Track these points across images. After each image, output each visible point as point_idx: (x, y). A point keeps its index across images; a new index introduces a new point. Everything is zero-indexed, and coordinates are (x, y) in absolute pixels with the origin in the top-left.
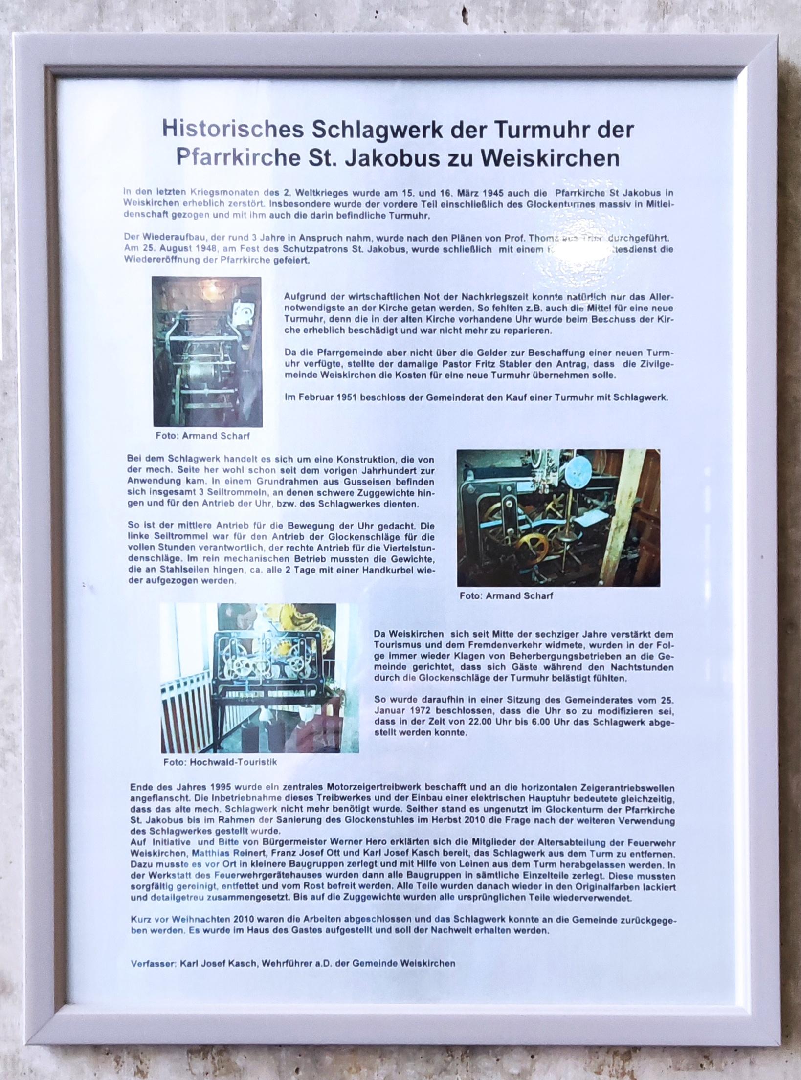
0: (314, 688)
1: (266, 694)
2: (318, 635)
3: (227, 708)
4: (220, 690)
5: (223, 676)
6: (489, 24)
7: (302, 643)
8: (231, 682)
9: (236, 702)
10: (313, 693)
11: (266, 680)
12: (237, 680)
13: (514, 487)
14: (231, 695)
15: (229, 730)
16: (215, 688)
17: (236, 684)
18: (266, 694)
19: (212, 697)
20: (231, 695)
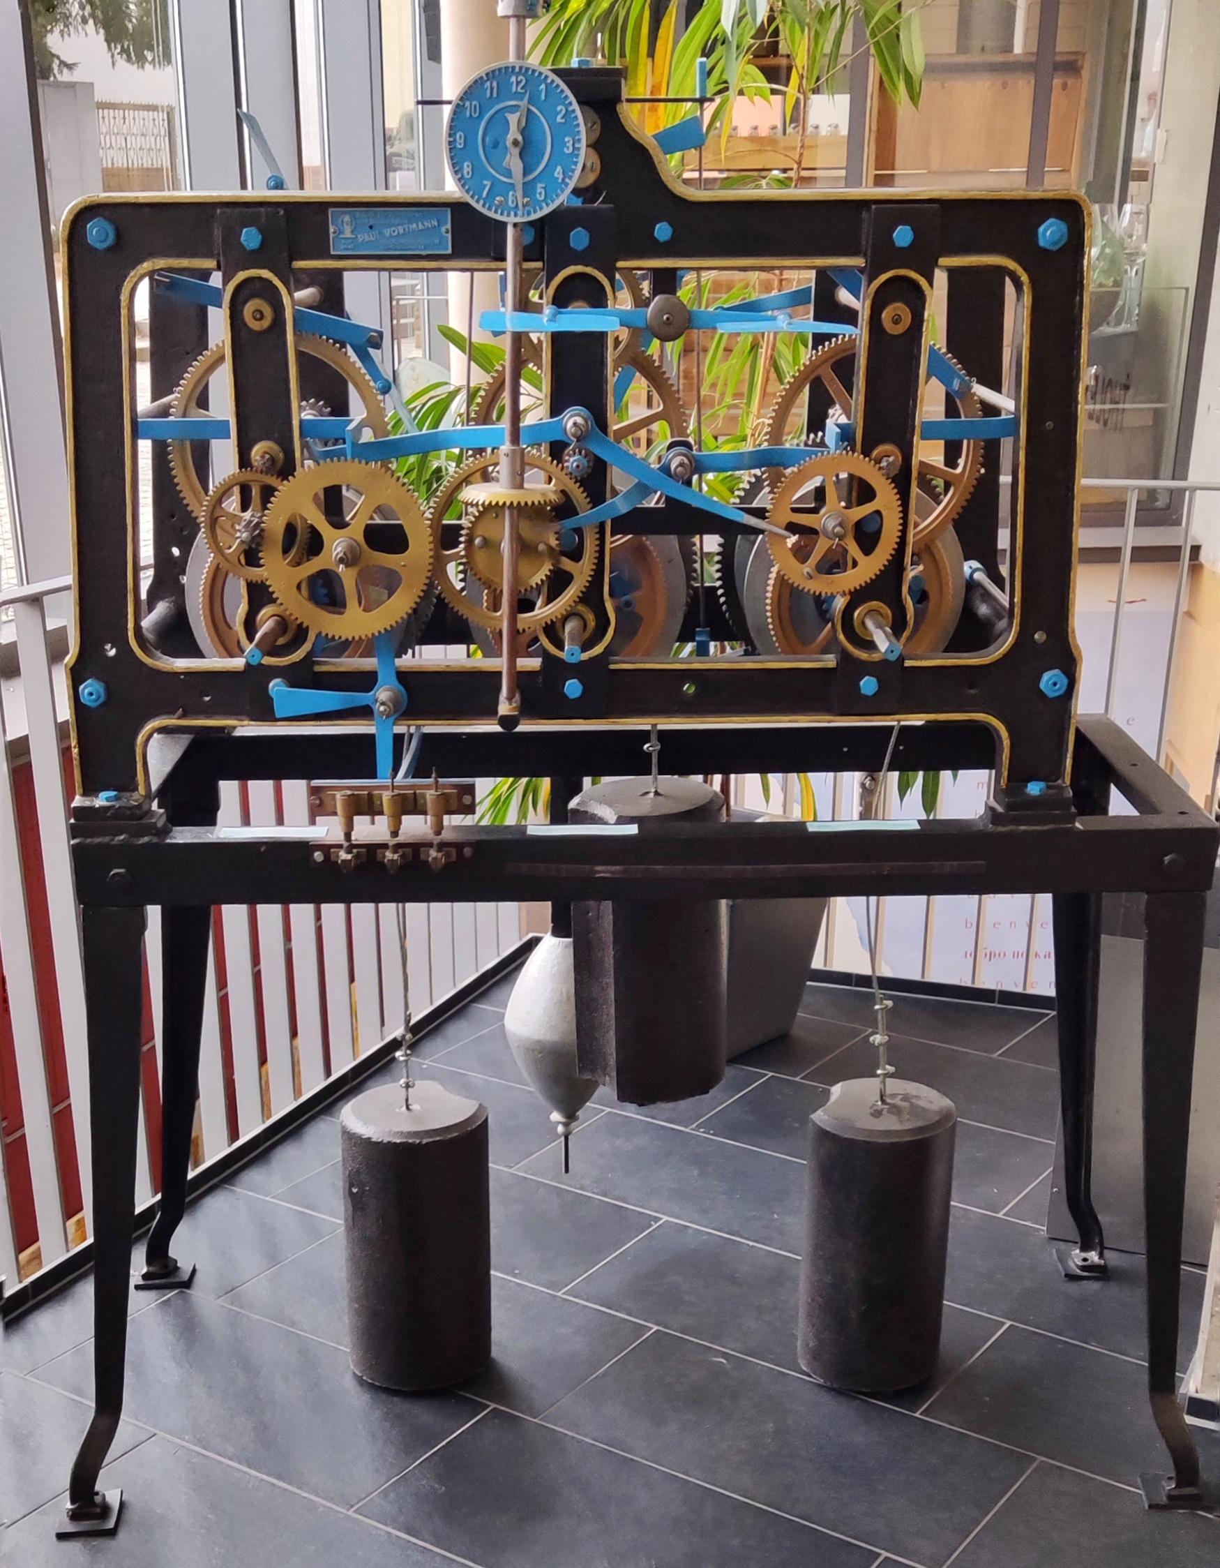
0: (968, 749)
1: (930, 431)
2: (1050, 232)
3: (233, 916)
4: (159, 756)
5: (176, 634)
6: (730, 136)
7: (895, 316)
8: (247, 692)
9: (285, 874)
10: (967, 795)
11: (555, 669)
12: (303, 676)
13: (654, 726)
14: (253, 814)
15: (283, 1107)
16: (98, 747)
17: (295, 715)
18: (930, 431)
19: (82, 823)
20: (253, 814)
